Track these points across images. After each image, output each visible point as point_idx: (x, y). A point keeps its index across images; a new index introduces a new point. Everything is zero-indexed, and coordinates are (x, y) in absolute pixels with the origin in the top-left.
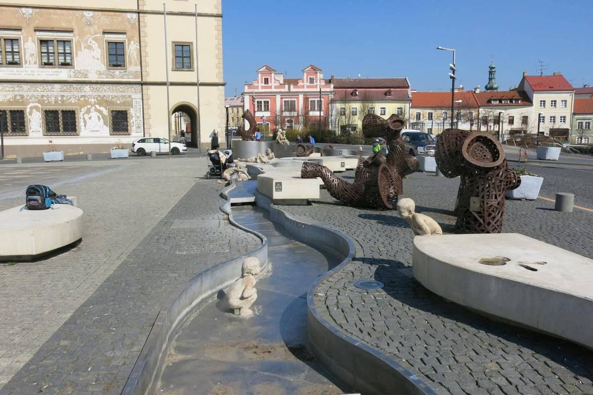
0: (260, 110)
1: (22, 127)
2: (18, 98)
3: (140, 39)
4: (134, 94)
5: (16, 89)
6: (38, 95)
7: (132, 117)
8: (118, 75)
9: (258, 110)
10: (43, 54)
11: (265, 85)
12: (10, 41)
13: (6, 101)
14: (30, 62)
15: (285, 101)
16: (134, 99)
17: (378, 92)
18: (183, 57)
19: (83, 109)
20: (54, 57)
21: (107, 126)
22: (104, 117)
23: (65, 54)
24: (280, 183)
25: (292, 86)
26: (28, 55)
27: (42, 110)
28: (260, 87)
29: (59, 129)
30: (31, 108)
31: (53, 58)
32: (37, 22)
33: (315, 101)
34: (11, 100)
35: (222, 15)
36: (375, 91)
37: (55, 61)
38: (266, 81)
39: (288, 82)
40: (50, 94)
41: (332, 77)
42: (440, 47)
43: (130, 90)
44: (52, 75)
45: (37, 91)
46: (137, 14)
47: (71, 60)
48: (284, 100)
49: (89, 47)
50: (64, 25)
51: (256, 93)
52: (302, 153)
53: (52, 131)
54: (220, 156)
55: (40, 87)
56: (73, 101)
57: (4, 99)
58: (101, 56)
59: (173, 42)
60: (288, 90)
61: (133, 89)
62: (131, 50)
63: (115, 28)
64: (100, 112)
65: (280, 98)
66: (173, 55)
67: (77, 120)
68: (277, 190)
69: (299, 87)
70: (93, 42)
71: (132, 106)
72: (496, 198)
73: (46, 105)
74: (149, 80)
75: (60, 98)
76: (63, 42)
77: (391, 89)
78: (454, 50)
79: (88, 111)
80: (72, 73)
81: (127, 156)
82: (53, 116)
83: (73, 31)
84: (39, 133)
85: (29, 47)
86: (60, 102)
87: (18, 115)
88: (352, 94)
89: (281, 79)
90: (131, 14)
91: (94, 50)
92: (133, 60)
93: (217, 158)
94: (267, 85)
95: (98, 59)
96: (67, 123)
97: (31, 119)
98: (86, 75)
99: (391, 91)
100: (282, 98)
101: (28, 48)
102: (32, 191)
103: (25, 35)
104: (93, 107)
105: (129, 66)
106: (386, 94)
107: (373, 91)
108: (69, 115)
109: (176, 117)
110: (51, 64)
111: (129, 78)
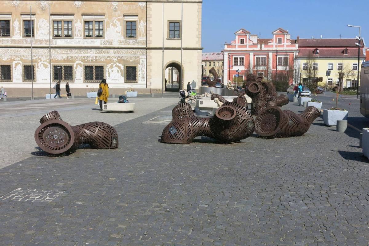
0: (236, 64)
1: (71, 77)
2: (70, 58)
3: (147, 19)
4: (141, 55)
5: (69, 52)
6: (81, 56)
7: (139, 71)
8: (131, 43)
9: (235, 65)
10: (86, 30)
11: (242, 45)
12: (67, 22)
13: (62, 60)
14: (78, 35)
15: (257, 58)
16: (141, 58)
17: (337, 50)
18: (174, 31)
19: (108, 66)
20: (93, 32)
21: (123, 77)
22: (121, 70)
23: (99, 29)
24: (202, 101)
25: (263, 46)
26: (77, 30)
27: (83, 66)
28: (237, 46)
29: (93, 78)
30: (77, 64)
31: (91, 32)
32: (84, 9)
33: (282, 58)
34: (65, 59)
35: (202, 1)
36: (334, 50)
37: (93, 34)
38: (242, 42)
39: (261, 42)
40: (89, 55)
41: (298, 38)
42: (349, 25)
43: (138, 53)
44: (90, 43)
45: (81, 53)
46: (146, 3)
47: (103, 33)
48: (256, 56)
49: (115, 25)
50: (100, 11)
51: (231, 51)
52: (237, 94)
53: (89, 79)
54: (185, 93)
55: (83, 51)
56: (103, 60)
57: (61, 58)
58: (121, 30)
59: (168, 21)
60: (260, 49)
61: (141, 52)
62: (141, 26)
63: (130, 12)
64: (119, 67)
65: (253, 55)
66: (168, 29)
67: (104, 72)
68: (201, 104)
69: (270, 46)
70: (117, 21)
71: (139, 63)
72: (260, 103)
73: (86, 62)
74: (152, 46)
75: (94, 58)
76: (98, 22)
77: (348, 48)
78: (360, 27)
79: (112, 67)
80: (103, 42)
81: (136, 96)
82: (90, 70)
83: (105, 15)
84: (81, 80)
85: (78, 26)
86: (94, 61)
87: (69, 69)
88: (314, 52)
89: (255, 40)
90: (142, 3)
91: (117, 27)
92: (141, 33)
93: (183, 94)
94: (243, 45)
95: (119, 33)
96: (98, 74)
97: (76, 71)
98: (112, 43)
99: (347, 49)
100: (254, 56)
101: (77, 27)
102: (121, 97)
103: (76, 18)
104: (115, 64)
105: (139, 37)
106: (343, 52)
107: (332, 50)
108: (99, 69)
109: (169, 70)
110: (90, 36)
111: (138, 45)
